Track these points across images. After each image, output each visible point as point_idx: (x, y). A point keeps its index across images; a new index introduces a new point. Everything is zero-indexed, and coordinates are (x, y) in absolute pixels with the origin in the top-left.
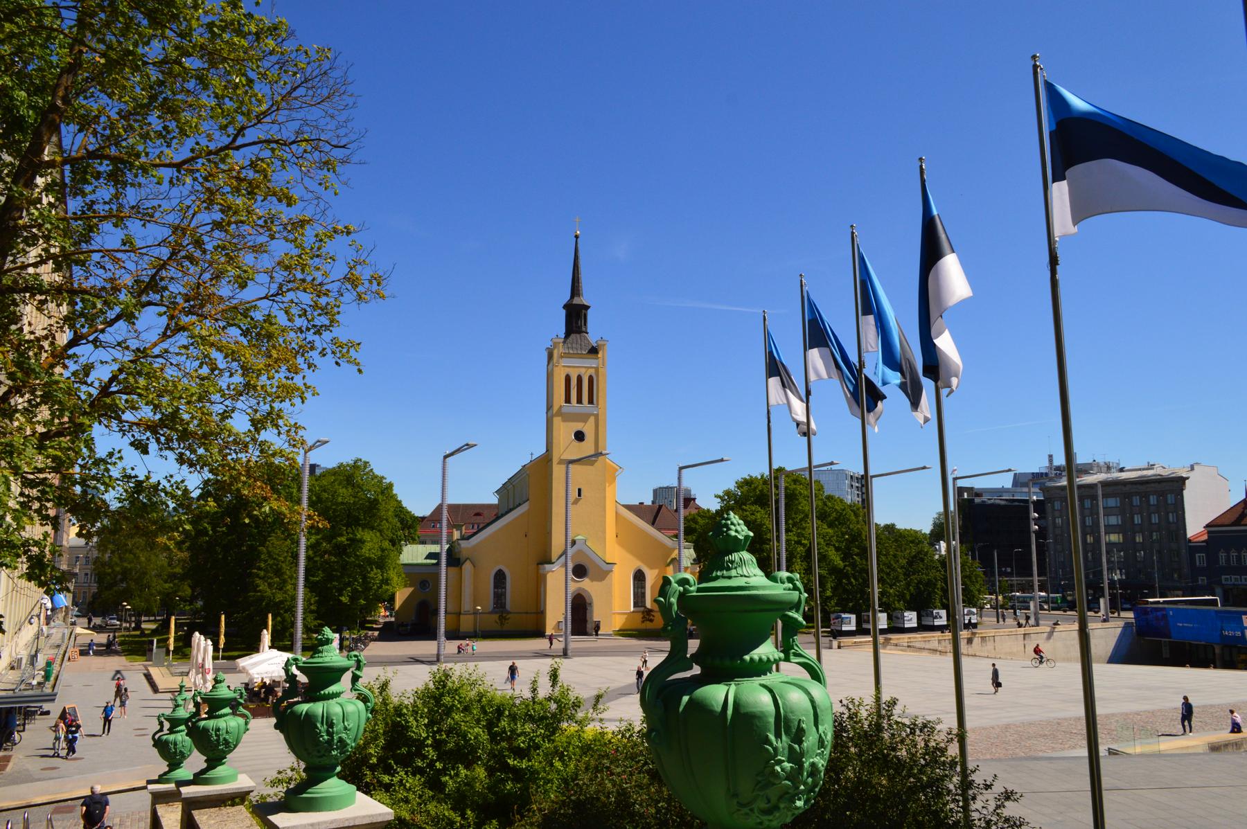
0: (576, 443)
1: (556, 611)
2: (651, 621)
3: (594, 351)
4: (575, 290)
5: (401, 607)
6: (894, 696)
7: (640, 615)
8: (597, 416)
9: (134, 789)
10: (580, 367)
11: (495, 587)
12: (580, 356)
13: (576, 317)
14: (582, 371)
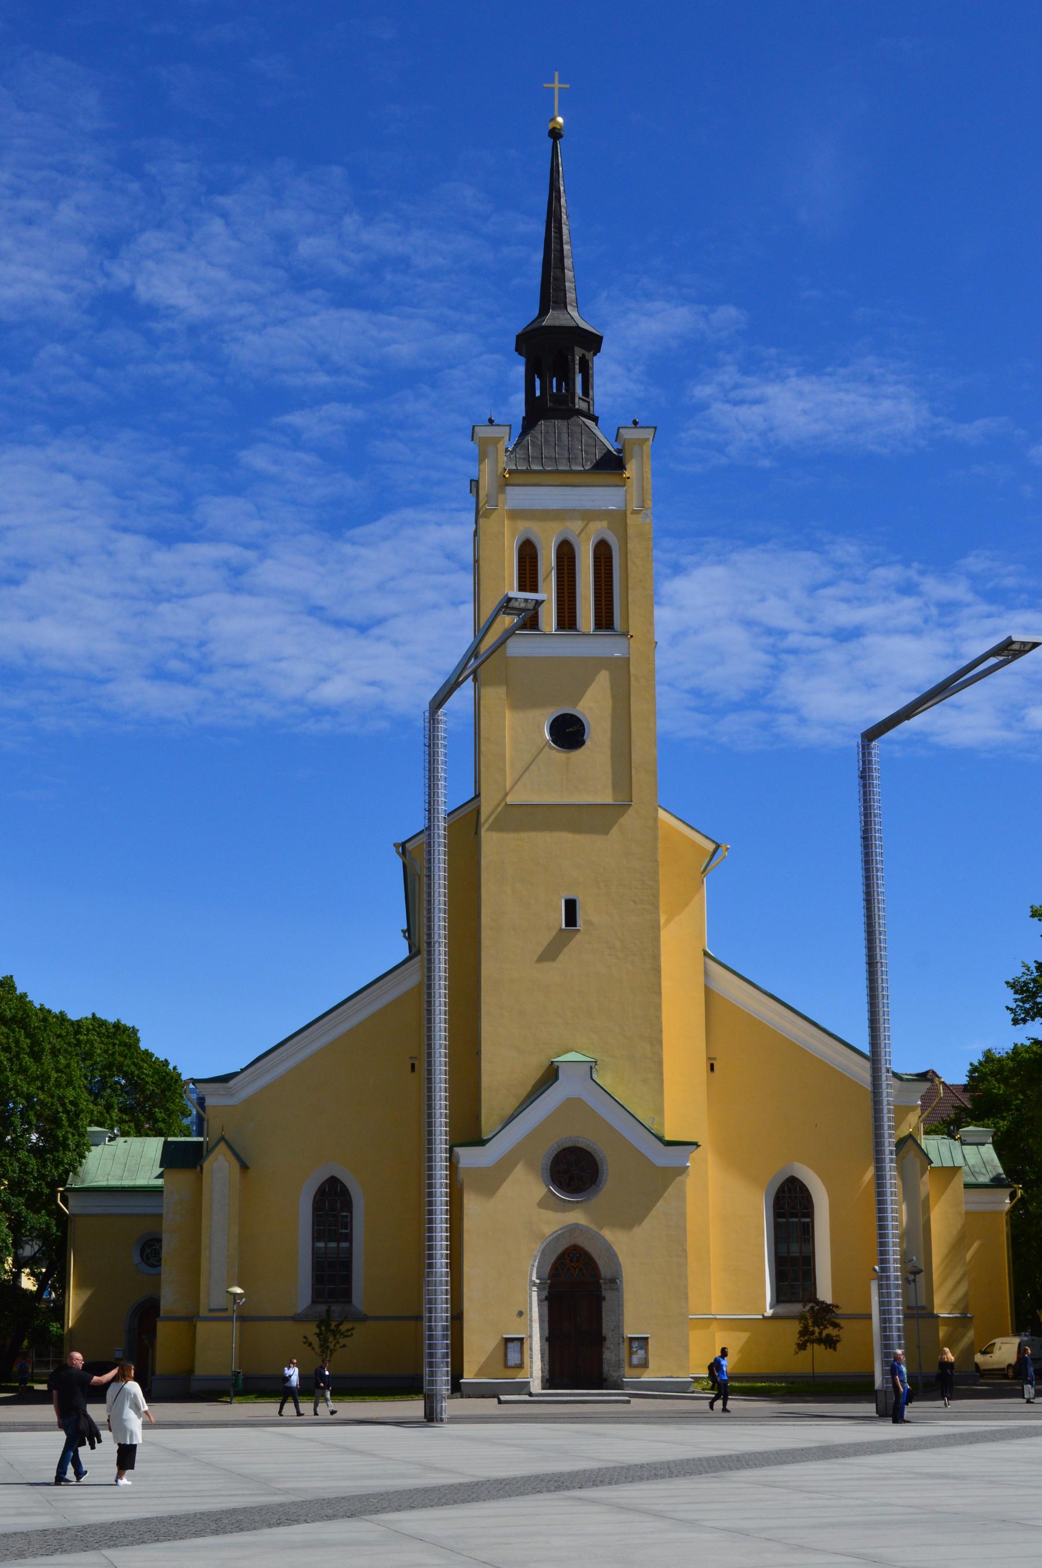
0: (559, 755)
1: (504, 1304)
2: (831, 1343)
3: (611, 464)
4: (552, 293)
5: (79, 1321)
6: (985, 1048)
7: (794, 1328)
8: (621, 672)
9: (689, 826)
10: (567, 510)
11: (318, 1235)
12: (564, 477)
13: (555, 356)
14: (573, 528)
